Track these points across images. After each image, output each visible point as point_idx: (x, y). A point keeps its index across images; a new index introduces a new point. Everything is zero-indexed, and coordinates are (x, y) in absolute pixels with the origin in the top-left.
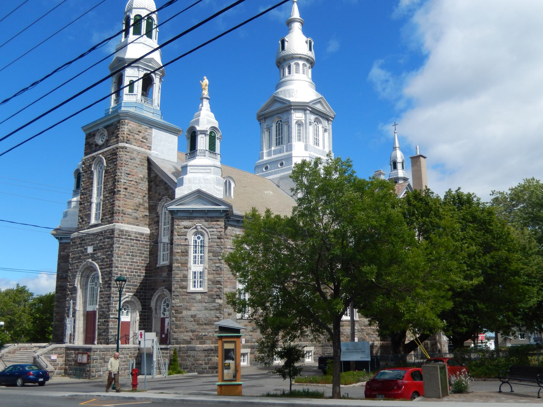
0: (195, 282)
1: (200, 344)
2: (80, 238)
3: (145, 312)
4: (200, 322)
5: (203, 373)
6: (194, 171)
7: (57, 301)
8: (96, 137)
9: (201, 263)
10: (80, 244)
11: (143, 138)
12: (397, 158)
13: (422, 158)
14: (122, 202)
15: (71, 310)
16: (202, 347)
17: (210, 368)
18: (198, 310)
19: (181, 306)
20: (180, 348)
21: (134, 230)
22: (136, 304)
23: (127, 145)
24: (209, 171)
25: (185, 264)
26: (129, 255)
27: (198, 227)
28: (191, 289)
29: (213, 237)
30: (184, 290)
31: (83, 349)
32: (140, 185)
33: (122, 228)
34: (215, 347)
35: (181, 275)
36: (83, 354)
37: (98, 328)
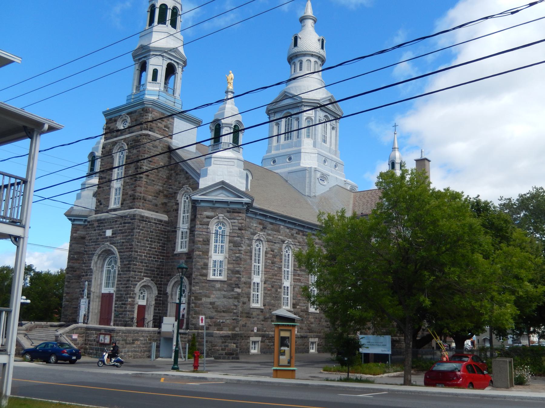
0: (215, 270)
1: (218, 330)
2: (98, 220)
3: (160, 297)
4: (219, 309)
5: (219, 358)
6: (218, 163)
7: (68, 282)
8: (118, 123)
9: (221, 253)
10: (97, 226)
11: (165, 127)
12: (395, 158)
13: (426, 162)
14: (143, 189)
15: (86, 291)
16: (219, 333)
17: (226, 354)
18: (216, 297)
19: (201, 293)
20: (198, 333)
21: (154, 217)
22: (153, 289)
23: (150, 133)
24: (232, 164)
25: (206, 253)
26: (148, 241)
27: (220, 217)
28: (211, 277)
29: (234, 228)
30: (204, 278)
31: (105, 330)
32: (161, 172)
33: (142, 214)
34: (232, 334)
35: (202, 263)
36: (105, 334)
37: (115, 310)
